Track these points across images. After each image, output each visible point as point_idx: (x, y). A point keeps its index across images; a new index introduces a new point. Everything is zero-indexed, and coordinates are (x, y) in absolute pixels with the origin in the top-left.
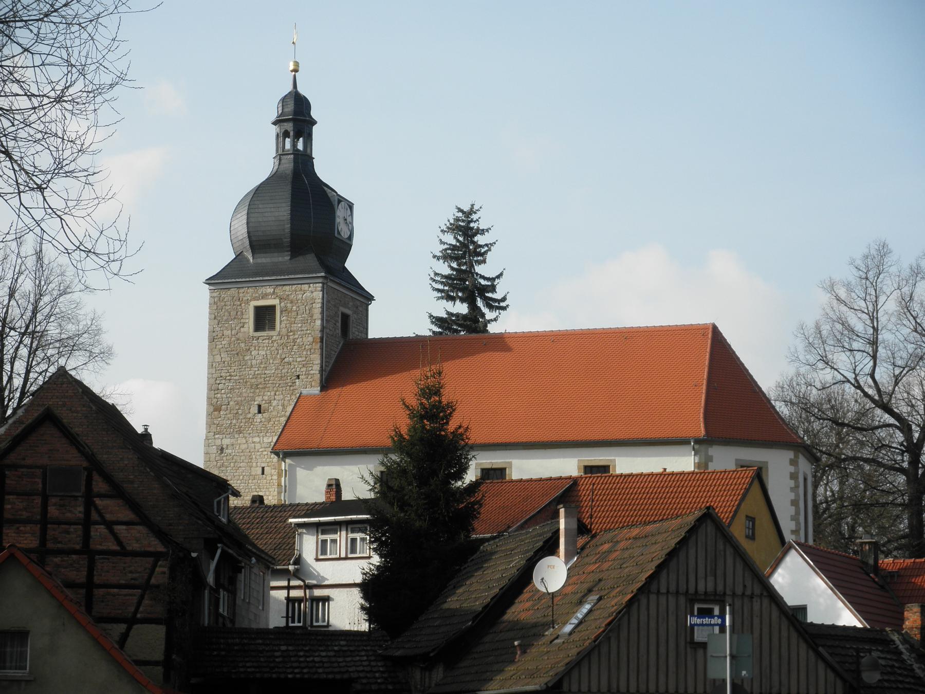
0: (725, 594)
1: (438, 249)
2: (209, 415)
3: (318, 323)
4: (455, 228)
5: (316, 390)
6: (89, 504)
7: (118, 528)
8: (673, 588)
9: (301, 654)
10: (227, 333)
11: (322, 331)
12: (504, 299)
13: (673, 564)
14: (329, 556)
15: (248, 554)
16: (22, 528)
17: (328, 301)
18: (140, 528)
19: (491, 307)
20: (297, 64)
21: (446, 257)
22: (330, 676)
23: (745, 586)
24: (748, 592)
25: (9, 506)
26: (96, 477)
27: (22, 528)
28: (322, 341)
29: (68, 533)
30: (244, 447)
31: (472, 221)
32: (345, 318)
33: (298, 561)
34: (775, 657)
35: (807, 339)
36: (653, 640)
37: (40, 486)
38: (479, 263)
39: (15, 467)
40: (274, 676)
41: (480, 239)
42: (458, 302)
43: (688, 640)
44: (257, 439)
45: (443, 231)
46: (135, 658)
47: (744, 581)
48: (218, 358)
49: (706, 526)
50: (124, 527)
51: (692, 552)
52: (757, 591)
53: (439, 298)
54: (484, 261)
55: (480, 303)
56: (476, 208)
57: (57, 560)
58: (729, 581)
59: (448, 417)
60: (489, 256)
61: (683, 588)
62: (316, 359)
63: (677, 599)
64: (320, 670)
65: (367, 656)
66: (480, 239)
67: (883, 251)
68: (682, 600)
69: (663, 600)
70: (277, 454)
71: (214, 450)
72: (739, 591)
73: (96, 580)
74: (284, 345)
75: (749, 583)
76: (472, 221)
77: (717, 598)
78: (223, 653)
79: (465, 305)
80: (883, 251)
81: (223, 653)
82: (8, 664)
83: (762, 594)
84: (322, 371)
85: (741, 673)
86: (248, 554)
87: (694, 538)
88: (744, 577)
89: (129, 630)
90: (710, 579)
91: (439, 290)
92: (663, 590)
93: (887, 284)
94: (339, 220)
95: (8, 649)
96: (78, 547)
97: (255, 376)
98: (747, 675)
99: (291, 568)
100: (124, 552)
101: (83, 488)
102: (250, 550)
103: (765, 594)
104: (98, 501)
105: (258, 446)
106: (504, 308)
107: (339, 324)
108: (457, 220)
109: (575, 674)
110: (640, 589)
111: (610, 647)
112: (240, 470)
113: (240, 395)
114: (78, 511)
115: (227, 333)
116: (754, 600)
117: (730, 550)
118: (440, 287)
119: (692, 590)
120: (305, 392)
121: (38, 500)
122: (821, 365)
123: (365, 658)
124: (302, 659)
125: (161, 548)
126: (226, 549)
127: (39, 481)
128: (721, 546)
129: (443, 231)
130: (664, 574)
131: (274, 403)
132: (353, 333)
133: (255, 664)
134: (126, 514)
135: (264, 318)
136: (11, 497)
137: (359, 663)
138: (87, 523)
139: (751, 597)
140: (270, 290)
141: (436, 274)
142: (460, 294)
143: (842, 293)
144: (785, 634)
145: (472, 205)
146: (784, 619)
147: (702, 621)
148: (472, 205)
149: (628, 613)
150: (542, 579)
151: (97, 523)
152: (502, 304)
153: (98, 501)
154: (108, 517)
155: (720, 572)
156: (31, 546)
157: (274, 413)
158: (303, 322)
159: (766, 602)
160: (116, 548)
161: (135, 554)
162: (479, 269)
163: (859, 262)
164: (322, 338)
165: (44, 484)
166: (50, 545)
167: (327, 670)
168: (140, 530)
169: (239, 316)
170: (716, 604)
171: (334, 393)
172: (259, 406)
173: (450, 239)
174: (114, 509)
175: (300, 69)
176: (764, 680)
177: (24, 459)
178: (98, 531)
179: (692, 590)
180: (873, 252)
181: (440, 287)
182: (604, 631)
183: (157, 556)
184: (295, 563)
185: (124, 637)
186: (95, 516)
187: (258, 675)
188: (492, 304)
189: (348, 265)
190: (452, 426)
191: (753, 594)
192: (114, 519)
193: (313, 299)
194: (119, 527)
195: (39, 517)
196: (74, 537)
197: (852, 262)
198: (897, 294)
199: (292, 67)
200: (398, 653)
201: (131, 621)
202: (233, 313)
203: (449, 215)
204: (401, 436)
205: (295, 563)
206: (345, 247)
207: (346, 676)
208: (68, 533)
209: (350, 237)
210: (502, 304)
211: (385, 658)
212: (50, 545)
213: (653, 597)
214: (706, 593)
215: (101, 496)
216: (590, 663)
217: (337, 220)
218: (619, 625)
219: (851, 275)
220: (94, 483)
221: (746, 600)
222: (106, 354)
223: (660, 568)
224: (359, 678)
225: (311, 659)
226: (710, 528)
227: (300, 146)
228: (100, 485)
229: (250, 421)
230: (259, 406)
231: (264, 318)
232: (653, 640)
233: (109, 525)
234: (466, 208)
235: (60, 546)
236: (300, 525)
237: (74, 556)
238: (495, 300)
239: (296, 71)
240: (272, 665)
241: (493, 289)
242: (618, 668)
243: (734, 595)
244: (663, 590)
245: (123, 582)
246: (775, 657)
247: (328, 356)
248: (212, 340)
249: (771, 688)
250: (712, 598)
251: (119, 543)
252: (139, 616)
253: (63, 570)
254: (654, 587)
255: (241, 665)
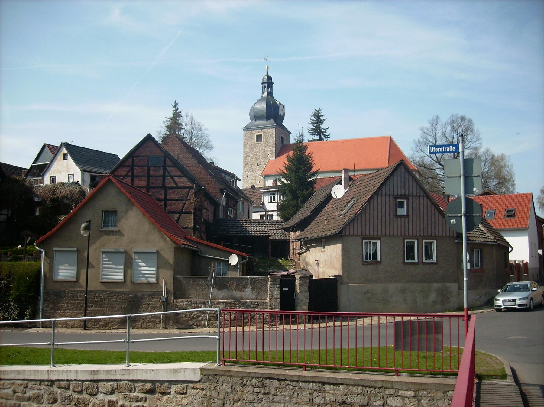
0: (409, 195)
1: (310, 121)
2: (244, 166)
3: (274, 139)
4: (315, 115)
5: (274, 158)
6: (165, 170)
7: (175, 178)
8: (388, 193)
9: (253, 227)
10: (249, 143)
11: (275, 141)
12: (329, 135)
13: (388, 183)
14: (273, 202)
15: (240, 197)
16: (141, 179)
17: (277, 133)
18: (184, 178)
19: (325, 137)
20: (268, 67)
21: (313, 124)
22: (262, 235)
23: (417, 192)
24: (418, 195)
25: (136, 171)
26: (167, 160)
27: (141, 179)
28: (275, 144)
29: (157, 180)
30: (254, 175)
31: (319, 113)
32: (282, 138)
33: (263, 203)
34: (429, 220)
35: (416, 144)
36: (380, 213)
37: (147, 163)
38: (321, 124)
39: (138, 156)
40: (242, 235)
41: (322, 118)
42: (316, 136)
43: (394, 214)
44: (257, 173)
45: (311, 116)
46: (182, 226)
47: (416, 190)
48: (246, 150)
49: (401, 168)
50: (178, 178)
51: (395, 178)
52: (422, 194)
53: (310, 135)
54: (323, 124)
55: (322, 136)
56: (320, 109)
57: (153, 190)
58: (411, 190)
59: (305, 151)
60: (324, 122)
61: (392, 193)
62: (274, 149)
63: (389, 197)
64: (259, 233)
65: (276, 228)
66: (322, 118)
67: (437, 118)
68: (391, 198)
69: (384, 198)
70: (262, 176)
71: (245, 176)
72: (415, 194)
73: (168, 197)
74: (265, 146)
75: (418, 191)
76: (319, 113)
77: (406, 197)
78: (225, 227)
79: (318, 136)
80: (437, 118)
81: (225, 227)
82: (110, 224)
83: (424, 196)
84: (275, 152)
85: (473, 189)
86: (240, 197)
87: (396, 173)
88: (416, 188)
89: (180, 216)
90: (403, 189)
91: (310, 133)
92: (384, 194)
93: (439, 127)
94: (280, 110)
95: (110, 218)
96: (161, 185)
97: (257, 155)
98: (477, 191)
99: (261, 205)
100: (177, 187)
101: (162, 164)
102: (241, 196)
103: (425, 195)
104: (168, 168)
105: (258, 175)
106: (329, 138)
107: (281, 140)
108: (315, 113)
109: (348, 227)
110: (374, 193)
111: (362, 217)
112: (253, 182)
113: (253, 160)
114: (161, 172)
115: (249, 143)
116: (421, 198)
117: (410, 177)
118: (311, 132)
119: (395, 194)
120: (270, 159)
121: (146, 168)
122: (420, 151)
123: (274, 229)
124: (252, 229)
125: (191, 186)
126: (227, 192)
127: (146, 161)
128: (407, 175)
129: (311, 116)
130: (384, 187)
131: (262, 162)
132: (285, 142)
133: (236, 231)
134: (179, 173)
135: (259, 138)
136: (136, 167)
137: (272, 230)
138: (164, 177)
139: (420, 197)
140: (261, 130)
141: (309, 128)
142: (316, 133)
143: (426, 131)
144: (433, 211)
145: (320, 109)
146: (432, 205)
147: (440, 150)
148: (320, 109)
149: (369, 203)
150: (335, 193)
151: (168, 177)
152: (329, 136)
153: (168, 168)
154: (172, 174)
155: (407, 186)
156: (144, 185)
157: (262, 165)
158: (270, 139)
159: (425, 199)
160: (174, 185)
161: (182, 188)
162: (322, 126)
163: (431, 121)
164: (275, 143)
165: (148, 162)
166: (150, 185)
167: (261, 233)
168: (184, 179)
169: (252, 138)
170: (405, 199)
171: (279, 158)
172: (258, 163)
173: (313, 118)
174: (174, 171)
175: (269, 68)
176: (425, 231)
177: (141, 154)
178: (168, 180)
179: (395, 194)
180: (435, 118)
181: (311, 132)
182: (359, 210)
183: (190, 188)
184: (262, 204)
185: (179, 218)
186: (167, 174)
187: (236, 235)
188: (325, 136)
189: (283, 123)
190: (307, 154)
191: (420, 195)
192: (174, 175)
193: (273, 132)
194: (176, 178)
195: (146, 175)
196: (159, 182)
197: (429, 121)
198: (441, 131)
199: (267, 68)
200: (285, 226)
201: (181, 213)
202: (250, 137)
203: (313, 111)
204: (290, 157)
205: (262, 204)
206: (282, 118)
207: (267, 235)
208: (157, 180)
209: (284, 115)
210: (329, 136)
211: (282, 228)
212: (150, 185)
213: (380, 197)
214: (401, 195)
215: (169, 166)
216: (354, 223)
217: (280, 110)
218: (366, 208)
219: (428, 125)
220: (166, 162)
221: (417, 198)
222: (211, 148)
223: (383, 184)
224: (272, 235)
225: (256, 229)
226: (402, 170)
227: (269, 90)
228: (168, 163)
229: (255, 168)
230: (258, 163)
231: (259, 138)
232: (380, 213)
233: (172, 177)
234: (318, 110)
235: (154, 185)
236: (263, 192)
237: (159, 189)
238: (327, 135)
239: (267, 69)
240: (242, 231)
241: (326, 132)
242: (366, 225)
243: (412, 196)
244: (384, 194)
245: (177, 198)
246: (429, 220)
247: (277, 148)
248: (244, 145)
249: (428, 234)
250: (404, 197)
251: (176, 184)
252: (183, 210)
253: (156, 194)
254: (380, 192)
255: (231, 231)
